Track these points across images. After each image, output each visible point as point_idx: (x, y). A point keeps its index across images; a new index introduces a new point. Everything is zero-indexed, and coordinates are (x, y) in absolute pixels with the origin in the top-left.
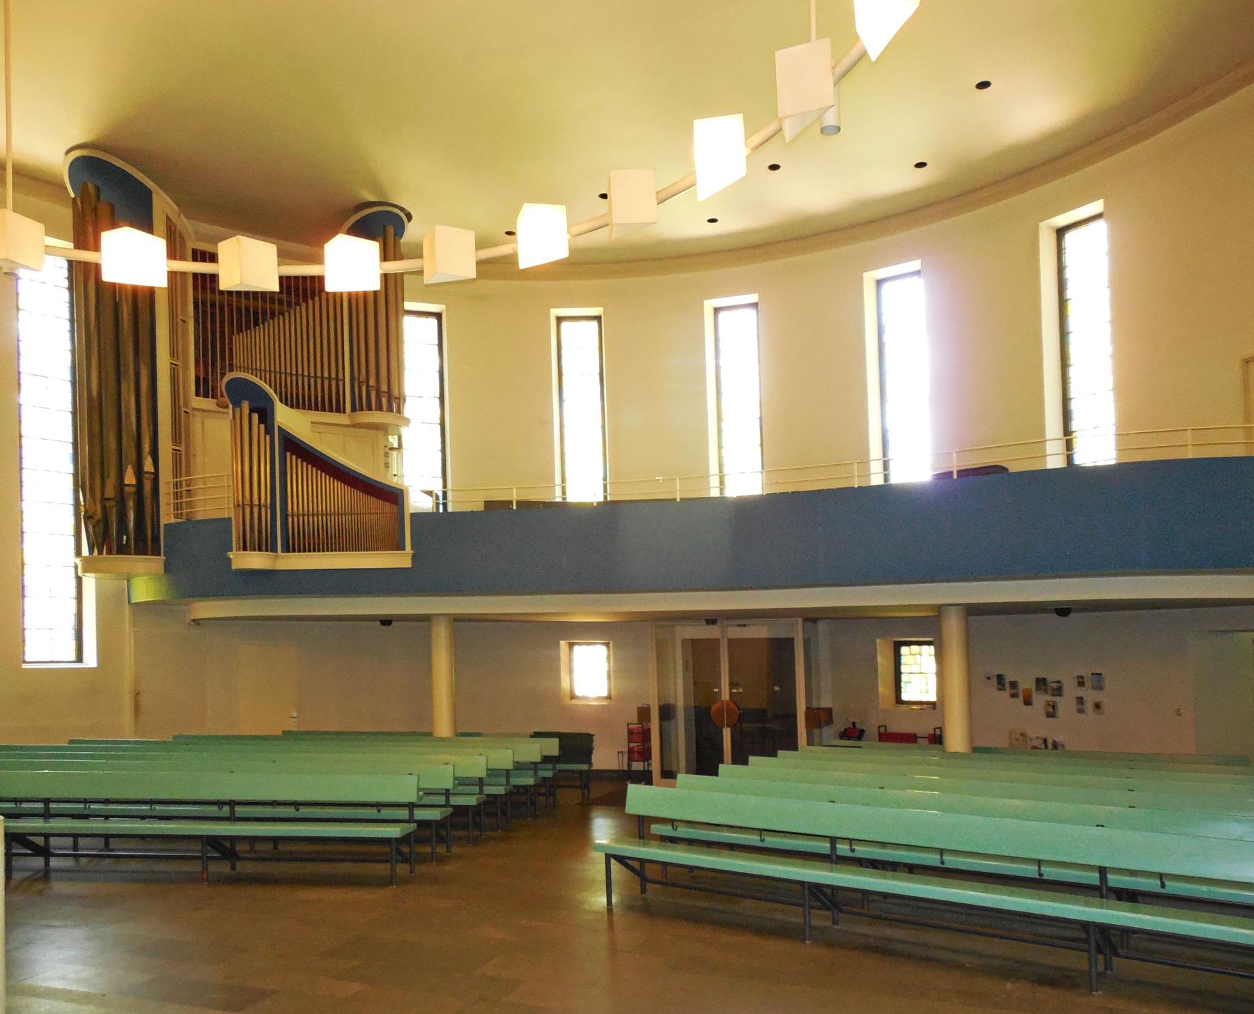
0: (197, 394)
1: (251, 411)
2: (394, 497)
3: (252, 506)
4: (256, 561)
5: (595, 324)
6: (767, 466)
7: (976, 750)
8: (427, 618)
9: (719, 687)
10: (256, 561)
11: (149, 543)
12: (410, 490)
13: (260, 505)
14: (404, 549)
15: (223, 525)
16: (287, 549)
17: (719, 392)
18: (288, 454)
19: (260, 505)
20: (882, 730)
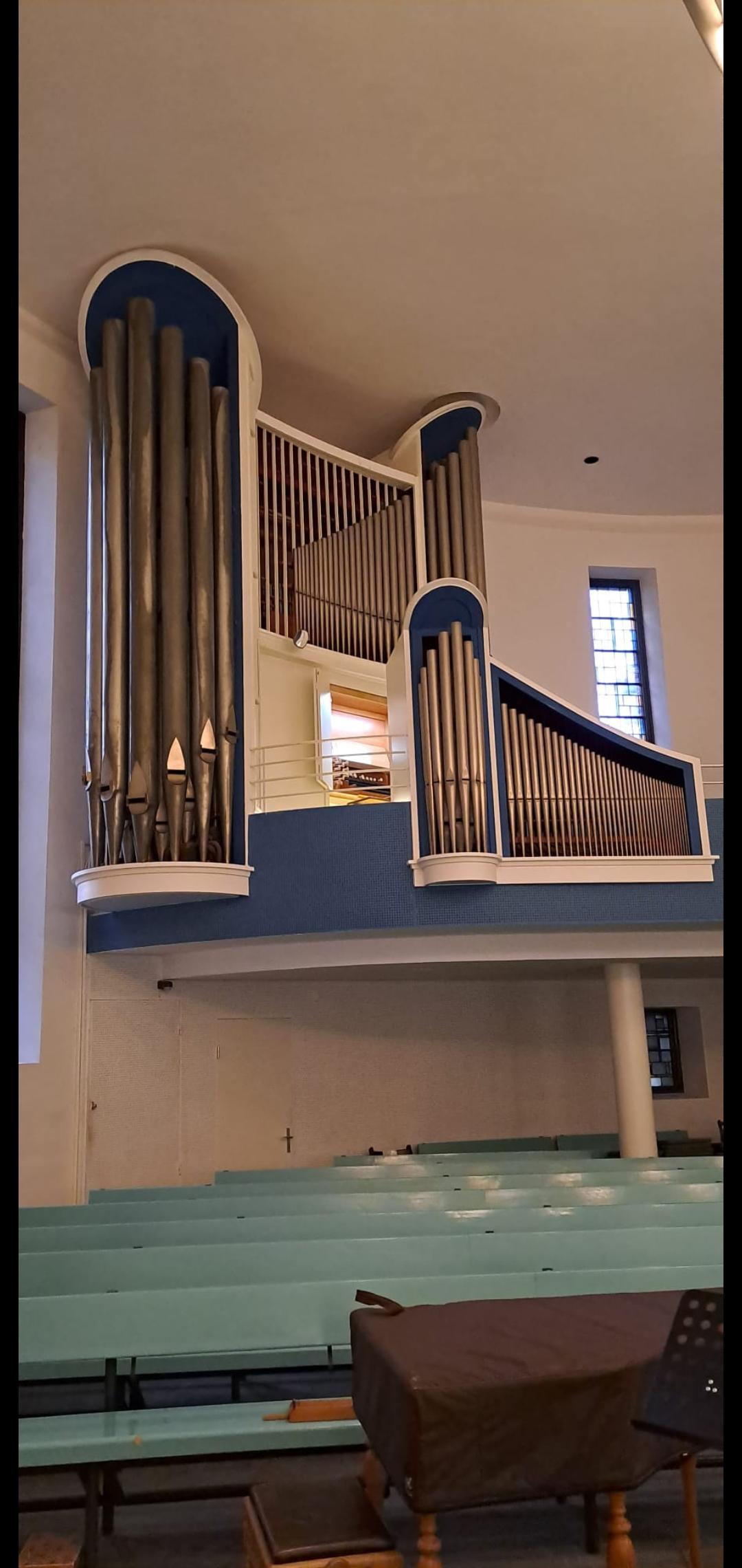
0: (264, 626)
1: (465, 638)
8: (597, 971)
16: (508, 852)
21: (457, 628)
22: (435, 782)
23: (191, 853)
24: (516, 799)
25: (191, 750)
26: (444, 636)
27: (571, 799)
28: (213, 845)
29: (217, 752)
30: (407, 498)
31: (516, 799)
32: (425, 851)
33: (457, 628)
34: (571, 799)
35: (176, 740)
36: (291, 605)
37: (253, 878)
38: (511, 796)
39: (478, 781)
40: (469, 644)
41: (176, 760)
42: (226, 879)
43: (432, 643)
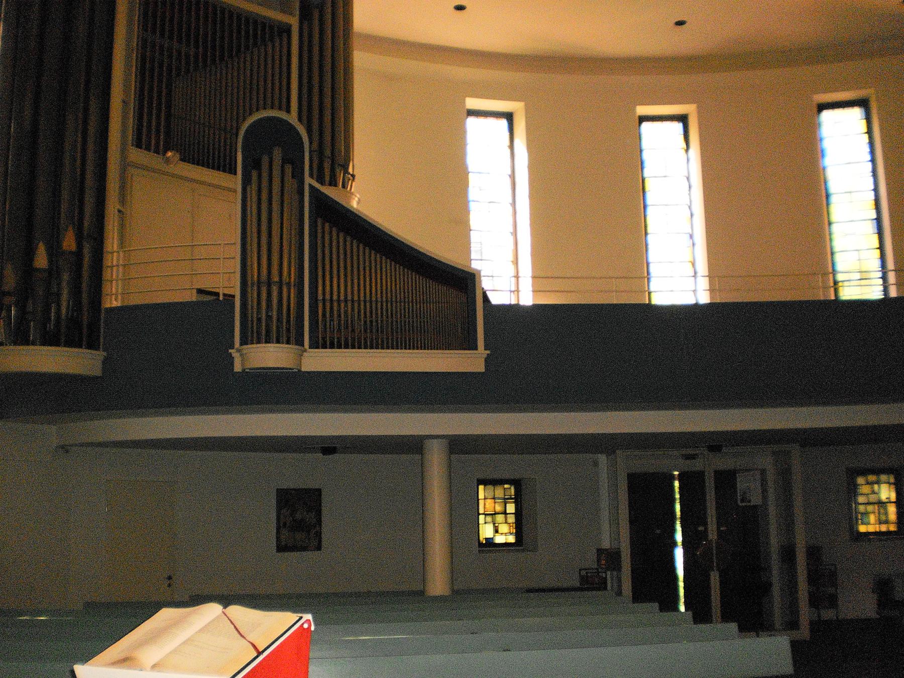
0: (139, 146)
1: (285, 161)
2: (463, 282)
3: (269, 284)
4: (271, 356)
5: (678, 127)
6: (712, 290)
7: (455, 592)
8: (414, 446)
9: (705, 524)
10: (271, 356)
11: (85, 330)
12: (482, 274)
13: (280, 282)
14: (475, 348)
15: (212, 305)
16: (314, 345)
17: (515, 233)
18: (319, 221)
19: (280, 282)
20: (583, 573)
21: (277, 154)
22: (253, 284)
23: (51, 339)
24: (324, 300)
25: (54, 251)
26: (265, 160)
27: (371, 302)
28: (77, 333)
29: (79, 254)
30: (285, 34)
31: (324, 300)
32: (244, 342)
33: (277, 154)
34: (371, 302)
35: (41, 244)
36: (168, 126)
37: (105, 362)
38: (320, 297)
39: (289, 284)
40: (289, 169)
41: (41, 260)
42: (470, 361)
43: (257, 165)
